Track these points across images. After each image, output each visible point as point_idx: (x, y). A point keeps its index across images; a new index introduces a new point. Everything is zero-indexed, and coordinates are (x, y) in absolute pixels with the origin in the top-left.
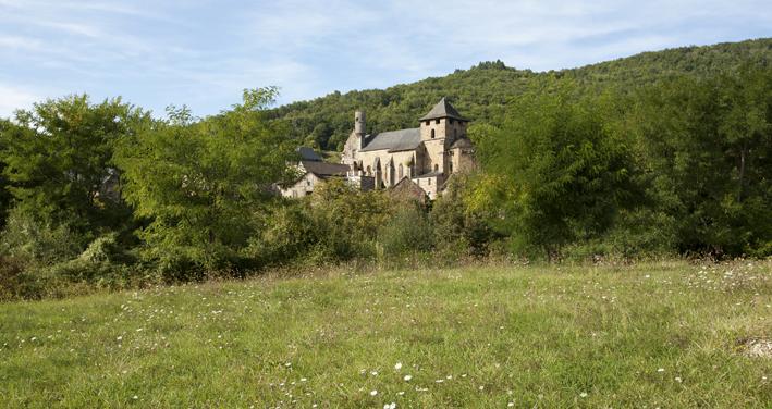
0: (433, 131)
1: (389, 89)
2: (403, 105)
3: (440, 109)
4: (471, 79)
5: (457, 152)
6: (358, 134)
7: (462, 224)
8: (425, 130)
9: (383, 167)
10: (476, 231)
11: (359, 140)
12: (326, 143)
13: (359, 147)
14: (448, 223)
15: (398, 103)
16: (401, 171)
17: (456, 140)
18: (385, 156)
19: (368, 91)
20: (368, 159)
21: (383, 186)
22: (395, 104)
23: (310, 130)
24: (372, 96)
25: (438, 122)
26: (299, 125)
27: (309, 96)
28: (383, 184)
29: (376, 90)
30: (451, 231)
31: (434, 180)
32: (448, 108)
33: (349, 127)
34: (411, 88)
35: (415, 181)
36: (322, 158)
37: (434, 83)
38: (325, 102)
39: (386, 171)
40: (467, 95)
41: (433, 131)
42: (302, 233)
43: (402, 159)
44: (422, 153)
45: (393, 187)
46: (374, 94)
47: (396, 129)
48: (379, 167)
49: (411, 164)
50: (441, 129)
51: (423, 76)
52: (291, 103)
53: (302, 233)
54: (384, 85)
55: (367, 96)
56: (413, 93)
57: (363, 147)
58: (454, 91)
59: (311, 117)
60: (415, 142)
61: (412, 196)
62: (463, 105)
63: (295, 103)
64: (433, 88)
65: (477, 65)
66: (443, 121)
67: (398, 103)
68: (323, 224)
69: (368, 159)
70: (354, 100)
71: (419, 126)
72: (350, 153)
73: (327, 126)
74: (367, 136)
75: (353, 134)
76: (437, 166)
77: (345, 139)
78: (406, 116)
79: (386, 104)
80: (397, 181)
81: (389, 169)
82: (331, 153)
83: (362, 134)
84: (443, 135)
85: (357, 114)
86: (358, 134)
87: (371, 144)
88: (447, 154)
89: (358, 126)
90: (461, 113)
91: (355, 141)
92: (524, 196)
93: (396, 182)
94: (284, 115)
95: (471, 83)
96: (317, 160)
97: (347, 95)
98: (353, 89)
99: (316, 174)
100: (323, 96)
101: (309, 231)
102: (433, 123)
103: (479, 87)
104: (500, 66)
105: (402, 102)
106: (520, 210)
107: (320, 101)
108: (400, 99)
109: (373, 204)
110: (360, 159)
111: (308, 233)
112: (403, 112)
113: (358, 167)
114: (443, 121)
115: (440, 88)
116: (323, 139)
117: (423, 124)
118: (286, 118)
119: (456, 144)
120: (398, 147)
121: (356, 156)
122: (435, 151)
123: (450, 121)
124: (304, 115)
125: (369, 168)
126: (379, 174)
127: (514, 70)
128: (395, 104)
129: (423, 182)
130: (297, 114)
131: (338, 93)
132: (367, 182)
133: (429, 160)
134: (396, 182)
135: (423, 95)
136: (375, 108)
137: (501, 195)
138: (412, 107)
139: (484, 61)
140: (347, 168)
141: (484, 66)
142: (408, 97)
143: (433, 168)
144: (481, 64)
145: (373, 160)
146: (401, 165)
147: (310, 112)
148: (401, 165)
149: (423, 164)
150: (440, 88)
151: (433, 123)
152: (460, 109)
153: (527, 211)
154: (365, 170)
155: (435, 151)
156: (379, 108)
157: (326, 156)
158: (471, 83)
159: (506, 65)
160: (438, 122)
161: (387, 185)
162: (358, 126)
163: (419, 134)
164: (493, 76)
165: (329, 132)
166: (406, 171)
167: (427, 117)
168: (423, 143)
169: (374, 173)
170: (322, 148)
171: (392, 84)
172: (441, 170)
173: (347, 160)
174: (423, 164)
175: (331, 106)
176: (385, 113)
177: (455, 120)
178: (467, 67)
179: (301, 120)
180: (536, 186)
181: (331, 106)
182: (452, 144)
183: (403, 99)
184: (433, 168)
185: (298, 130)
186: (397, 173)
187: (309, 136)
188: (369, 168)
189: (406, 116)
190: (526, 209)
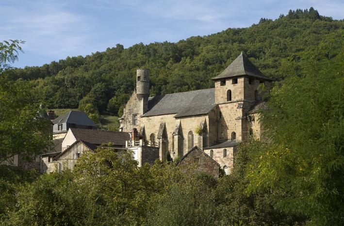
0: (229, 92)
1: (181, 42)
2: (198, 61)
3: (237, 66)
4: (278, 30)
5: (257, 116)
6: (140, 96)
7: (252, 205)
8: (220, 91)
9: (169, 135)
10: (270, 214)
11: (141, 104)
12: (105, 106)
13: (141, 112)
14: (235, 204)
15: (192, 59)
16: (191, 140)
17: (257, 102)
18: (171, 123)
19: (157, 44)
20: (151, 125)
21: (169, 158)
22: (188, 60)
23: (87, 91)
24: (161, 50)
25: (235, 82)
26: (73, 85)
27: (85, 50)
28: (169, 156)
29: (166, 44)
30: (239, 213)
31: (230, 151)
32: (248, 65)
33: (132, 87)
34: (208, 40)
35: (208, 152)
36: (100, 125)
37: (234, 36)
38: (104, 60)
39: (173, 140)
40: (274, 49)
41: (229, 92)
42: (53, 214)
43: (192, 125)
44: (216, 118)
45: (181, 157)
46: (133, 72)
47: (189, 89)
48: (164, 135)
49: (202, 132)
50: (238, 89)
51: (221, 27)
52: (64, 58)
53: (53, 214)
54: (174, 37)
55: (155, 51)
56: (210, 46)
57: (144, 112)
58: (259, 44)
59: (87, 75)
60: (208, 105)
61: (202, 170)
62: (270, 61)
63: (69, 58)
64: (234, 41)
65: (286, 14)
66: (241, 81)
67: (192, 59)
68: (79, 205)
69: (151, 125)
70: (139, 55)
71: (213, 87)
72: (130, 119)
73: (107, 86)
74: (150, 98)
75: (134, 95)
76: (234, 134)
77: (126, 100)
78: (201, 74)
79: (177, 60)
80: (186, 151)
81: (176, 137)
82: (110, 118)
83: (144, 96)
84: (242, 97)
85: (139, 72)
86: (140, 96)
87: (155, 107)
88: (246, 120)
89: (139, 87)
90: (264, 71)
91: (136, 104)
92: (316, 171)
93: (185, 154)
94: (55, 74)
95: (280, 35)
96: (90, 128)
97: (131, 48)
98: (138, 43)
99: (87, 144)
100: (102, 49)
101: (63, 213)
102: (229, 83)
103: (288, 39)
104: (313, 15)
105: (196, 58)
106: (311, 188)
107: (99, 56)
108: (194, 54)
109: (149, 180)
110: (142, 125)
111: (60, 216)
112: (198, 69)
113: (139, 135)
114: (241, 81)
115: (242, 41)
116: (101, 102)
117: (218, 84)
118: (58, 77)
119: (257, 108)
120: (189, 109)
121: (138, 123)
122: (232, 115)
123: (250, 80)
124: (79, 73)
125: (152, 136)
126: (165, 144)
127: (330, 19)
128: (188, 60)
129: (218, 154)
130: (72, 72)
131: (120, 47)
132: (149, 154)
133: (225, 127)
134: (185, 154)
135: (222, 50)
136: (164, 64)
137: (290, 170)
138: (208, 63)
139: (294, 9)
140: (126, 136)
141: (294, 15)
142: (205, 52)
143: (230, 137)
144: (291, 13)
145: (157, 127)
146: (191, 133)
147: (86, 70)
148: (191, 133)
149: (217, 132)
150: (242, 41)
151: (229, 83)
152: (265, 67)
153: (319, 190)
154: (148, 138)
155: (232, 115)
156: (168, 65)
157: (104, 122)
158: (280, 35)
159: (321, 14)
160: (235, 82)
161: (174, 156)
162: (139, 87)
163: (213, 96)
164: (305, 27)
165: (109, 93)
166: (197, 140)
167: (225, 73)
168: (217, 107)
169: (158, 142)
170: (101, 113)
171: (185, 37)
172: (239, 138)
173: (127, 127)
174: (217, 132)
175: (112, 63)
176: (176, 71)
177: (253, 77)
178: (274, 16)
179: (76, 79)
180: (329, 159)
181: (112, 63)
182: (252, 108)
183: (197, 54)
184: (230, 137)
185: (71, 90)
186: (186, 142)
187: (85, 98)
188: (152, 136)
189: (201, 74)
190: (318, 187)
